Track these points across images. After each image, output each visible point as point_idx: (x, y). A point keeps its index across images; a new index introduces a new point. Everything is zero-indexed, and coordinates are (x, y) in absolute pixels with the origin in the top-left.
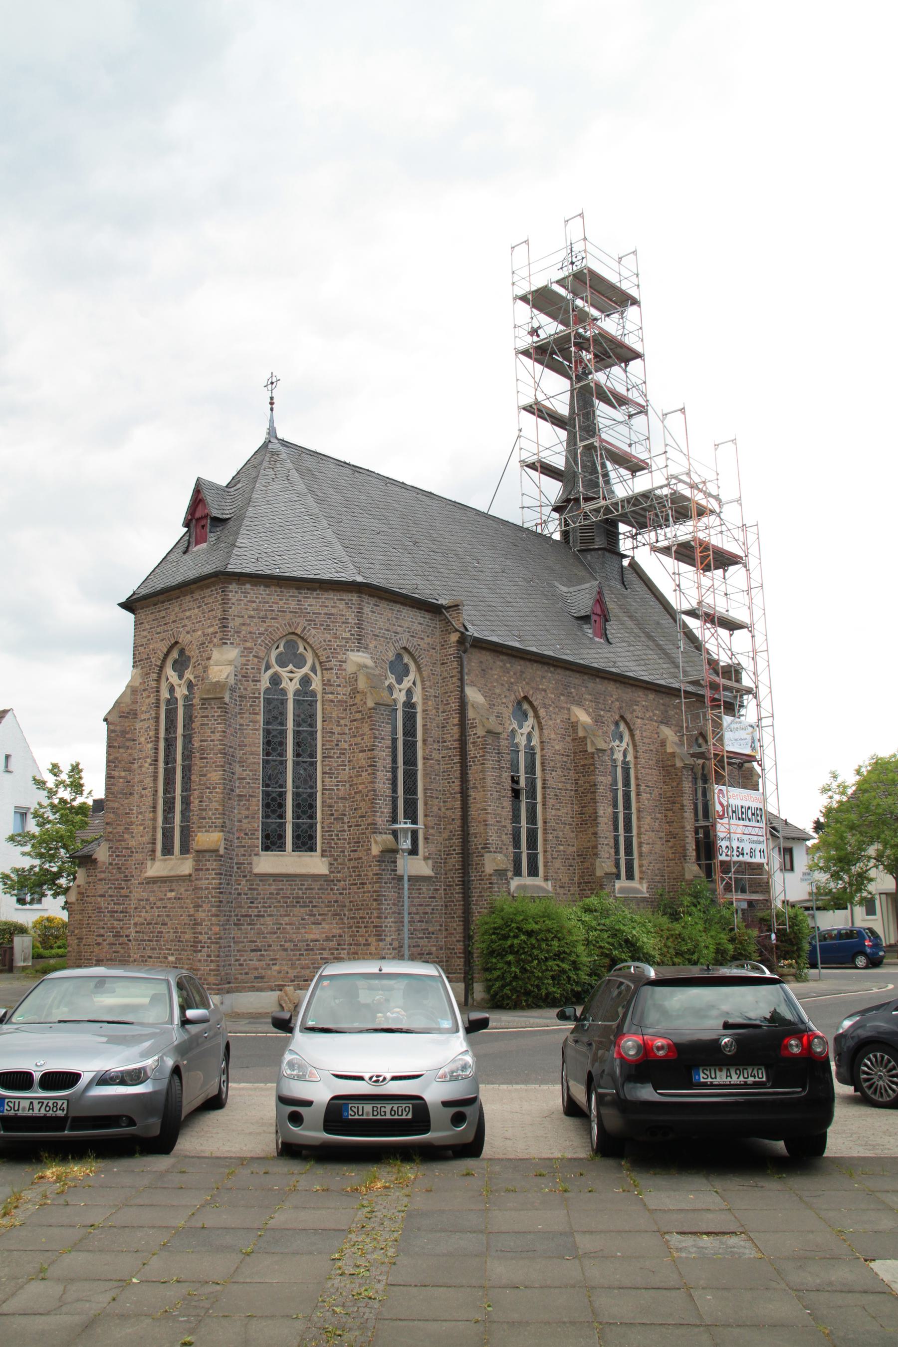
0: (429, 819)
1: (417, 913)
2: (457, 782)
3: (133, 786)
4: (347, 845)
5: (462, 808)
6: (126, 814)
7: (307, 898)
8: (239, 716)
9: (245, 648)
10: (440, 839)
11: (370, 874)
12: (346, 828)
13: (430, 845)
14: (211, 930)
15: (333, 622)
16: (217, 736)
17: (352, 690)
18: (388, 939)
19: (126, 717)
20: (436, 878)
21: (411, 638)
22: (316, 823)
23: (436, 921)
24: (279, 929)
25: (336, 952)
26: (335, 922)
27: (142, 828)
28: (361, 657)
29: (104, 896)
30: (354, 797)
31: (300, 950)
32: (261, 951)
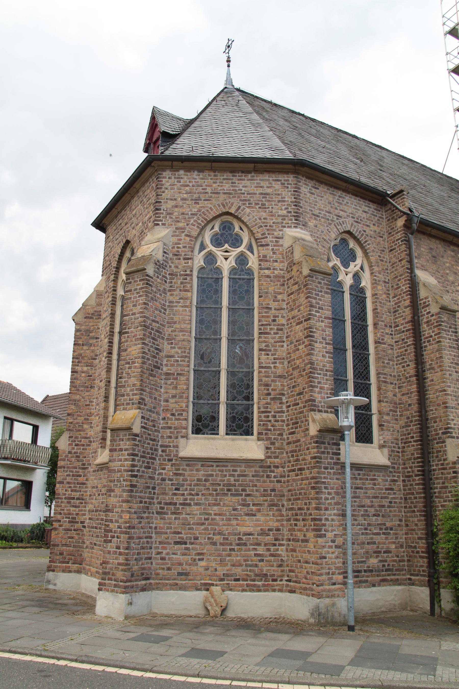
0: (383, 404)
1: (372, 506)
2: (412, 365)
3: (94, 380)
4: (285, 427)
5: (418, 392)
6: (86, 405)
7: (240, 485)
8: (168, 294)
9: (177, 228)
10: (397, 427)
11: (308, 457)
12: (284, 409)
13: (386, 433)
14: (122, 518)
15: (269, 201)
16: (138, 309)
17: (289, 263)
18: (330, 535)
19: (91, 318)
20: (394, 468)
21: (355, 224)
22: (253, 405)
23: (395, 516)
24: (207, 519)
25: (272, 548)
26: (271, 513)
27: (97, 418)
28: (296, 232)
29: (63, 483)
30: (292, 374)
31: (231, 544)
32: (185, 543)
